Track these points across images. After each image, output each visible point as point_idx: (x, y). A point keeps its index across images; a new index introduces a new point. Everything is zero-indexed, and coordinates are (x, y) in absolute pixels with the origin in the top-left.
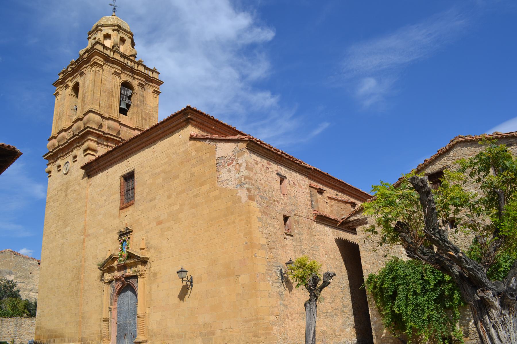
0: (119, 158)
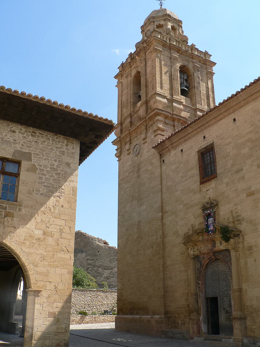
0: (193, 133)
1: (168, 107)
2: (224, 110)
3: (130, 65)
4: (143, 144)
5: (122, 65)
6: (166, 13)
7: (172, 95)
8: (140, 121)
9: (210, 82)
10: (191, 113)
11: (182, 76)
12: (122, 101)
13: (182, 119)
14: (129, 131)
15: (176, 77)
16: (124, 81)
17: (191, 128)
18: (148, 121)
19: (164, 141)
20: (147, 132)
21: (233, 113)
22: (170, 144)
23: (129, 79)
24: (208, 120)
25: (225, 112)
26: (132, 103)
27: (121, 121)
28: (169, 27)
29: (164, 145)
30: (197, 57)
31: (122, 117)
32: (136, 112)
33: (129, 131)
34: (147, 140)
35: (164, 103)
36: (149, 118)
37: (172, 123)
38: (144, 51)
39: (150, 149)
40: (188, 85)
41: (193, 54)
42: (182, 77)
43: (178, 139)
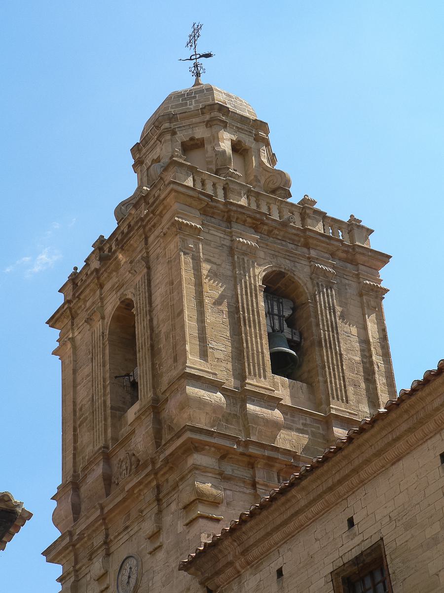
0: (314, 509)
1: (228, 418)
2: (405, 427)
3: (98, 278)
4: (150, 553)
5: (74, 279)
6: (210, 102)
7: (241, 376)
8: (137, 472)
9: (372, 321)
10: (313, 434)
11: (275, 308)
12: (74, 403)
13: (280, 456)
14: (102, 509)
15: (253, 315)
16: (82, 335)
17: (304, 493)
18: (162, 472)
19: (216, 543)
20: (160, 511)
21: (435, 434)
22: (239, 550)
23: (98, 326)
24: (356, 463)
25: (410, 430)
26: (109, 411)
27: (74, 476)
28: (225, 146)
29: (220, 556)
30: (323, 242)
31: (77, 460)
32: (123, 441)
33: (102, 509)
34: (163, 538)
35: (216, 408)
36: (166, 461)
37: (245, 474)
38: (141, 231)
39: (173, 571)
40: (296, 338)
41: (308, 233)
42: (276, 311)
43: (262, 533)
